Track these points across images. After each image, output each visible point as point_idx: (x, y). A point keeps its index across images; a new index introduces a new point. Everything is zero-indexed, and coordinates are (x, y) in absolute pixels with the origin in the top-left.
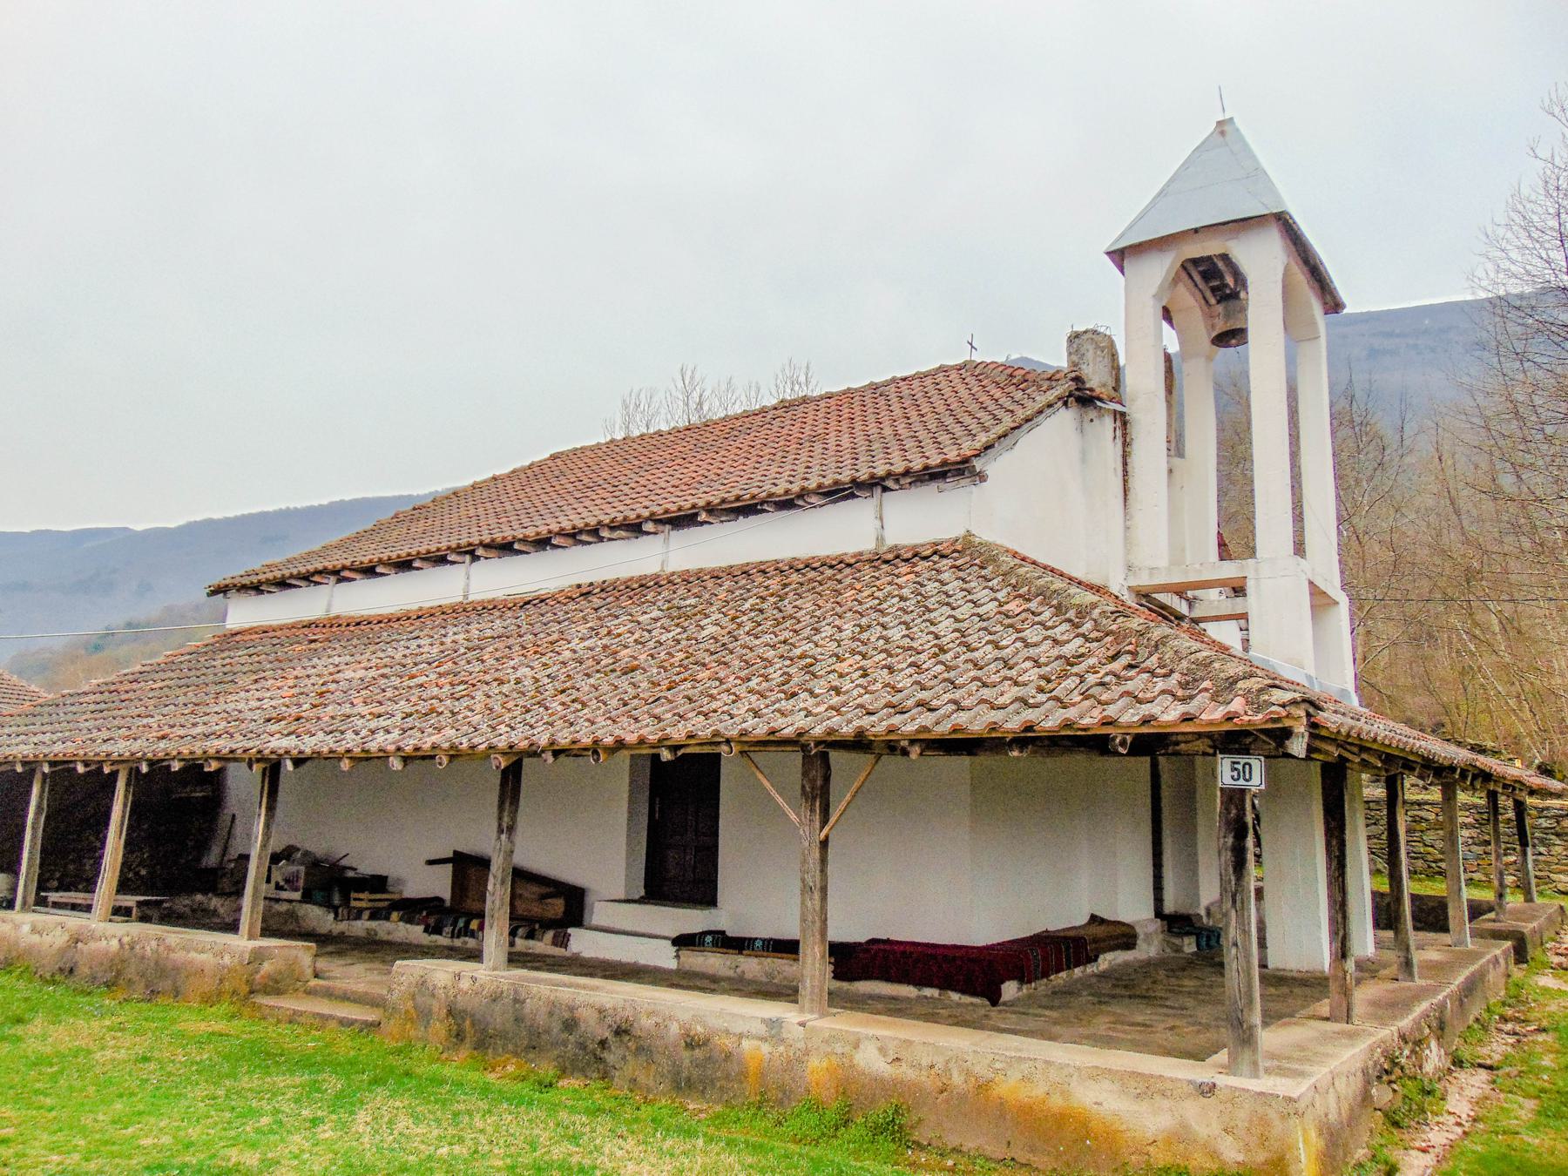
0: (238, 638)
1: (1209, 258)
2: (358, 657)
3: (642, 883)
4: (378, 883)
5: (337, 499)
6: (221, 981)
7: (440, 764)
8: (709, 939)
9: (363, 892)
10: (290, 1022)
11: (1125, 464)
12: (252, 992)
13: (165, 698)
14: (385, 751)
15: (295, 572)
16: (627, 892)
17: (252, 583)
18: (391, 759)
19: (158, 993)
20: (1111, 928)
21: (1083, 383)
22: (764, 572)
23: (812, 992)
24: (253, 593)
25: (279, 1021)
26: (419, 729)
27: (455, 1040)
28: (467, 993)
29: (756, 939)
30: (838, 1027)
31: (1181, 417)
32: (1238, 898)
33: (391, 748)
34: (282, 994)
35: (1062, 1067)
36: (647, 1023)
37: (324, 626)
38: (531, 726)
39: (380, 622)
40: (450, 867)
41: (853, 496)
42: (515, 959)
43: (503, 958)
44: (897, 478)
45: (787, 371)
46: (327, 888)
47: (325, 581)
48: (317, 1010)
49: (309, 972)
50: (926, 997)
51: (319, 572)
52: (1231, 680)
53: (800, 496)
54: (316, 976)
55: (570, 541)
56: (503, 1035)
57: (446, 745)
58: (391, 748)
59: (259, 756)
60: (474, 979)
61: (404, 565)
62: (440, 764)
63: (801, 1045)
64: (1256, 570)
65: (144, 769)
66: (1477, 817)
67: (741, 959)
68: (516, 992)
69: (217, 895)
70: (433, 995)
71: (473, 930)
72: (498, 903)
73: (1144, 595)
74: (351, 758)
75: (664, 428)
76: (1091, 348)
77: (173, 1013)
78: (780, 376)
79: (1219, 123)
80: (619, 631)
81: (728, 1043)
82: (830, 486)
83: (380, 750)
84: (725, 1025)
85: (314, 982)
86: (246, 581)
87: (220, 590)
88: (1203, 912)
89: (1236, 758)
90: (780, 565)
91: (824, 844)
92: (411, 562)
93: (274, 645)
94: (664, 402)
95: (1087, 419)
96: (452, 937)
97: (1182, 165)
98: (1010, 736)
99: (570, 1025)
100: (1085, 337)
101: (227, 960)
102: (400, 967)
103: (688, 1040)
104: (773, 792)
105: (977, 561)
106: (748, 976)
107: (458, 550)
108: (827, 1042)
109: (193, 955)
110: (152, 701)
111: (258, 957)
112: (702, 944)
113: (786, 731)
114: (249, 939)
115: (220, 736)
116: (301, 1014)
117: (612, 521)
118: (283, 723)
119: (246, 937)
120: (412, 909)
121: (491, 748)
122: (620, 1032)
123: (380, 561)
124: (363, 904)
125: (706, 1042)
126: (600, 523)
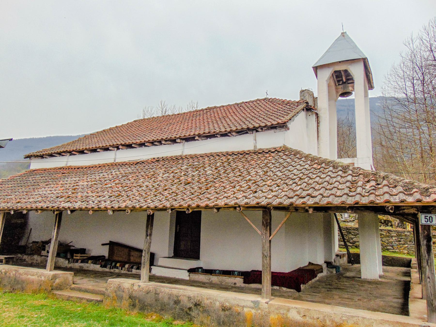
0: (36, 172)
1: (340, 71)
2: (81, 178)
3: (173, 252)
4: (83, 251)
5: (49, 136)
6: (40, 285)
7: (127, 213)
8: (200, 270)
9: (78, 254)
10: (68, 300)
11: (318, 129)
12: (52, 289)
13: (14, 190)
14: (107, 208)
15: (56, 152)
16: (169, 254)
17: (40, 155)
18: (108, 211)
19: (15, 289)
20: (316, 267)
21: (308, 104)
22: (218, 155)
23: (267, 292)
24: (40, 158)
25: (63, 300)
26: (117, 201)
27: (132, 307)
28: (136, 291)
29: (216, 270)
30: (281, 304)
32: (429, 261)
33: (109, 207)
34: (62, 290)
35: (369, 319)
36: (207, 302)
37: (66, 169)
38: (160, 201)
39: (86, 168)
40: (108, 246)
41: (247, 133)
42: (57, 268)
43: (147, 278)
45: (191, 104)
46: (65, 252)
47: (66, 155)
48: (78, 296)
49: (71, 282)
50: (275, 289)
51: (64, 152)
52: (426, 189)
53: (230, 132)
54: (74, 284)
55: (151, 144)
56: (151, 305)
57: (130, 206)
58: (109, 207)
59: (57, 209)
60: (139, 286)
61: (94, 150)
62: (127, 213)
63: (267, 310)
64: (357, 161)
65: (12, 213)
66: (397, 234)
67: (211, 277)
68: (156, 290)
69: (26, 254)
70: (123, 291)
71: (118, 267)
72: (146, 260)
74: (92, 210)
75: (170, 114)
76: (308, 95)
77: (24, 297)
78: (189, 105)
79: (342, 33)
80: (176, 171)
81: (239, 309)
82: (240, 129)
83: (226, 205)
84: (237, 303)
85: (73, 286)
86: (39, 154)
87: (29, 157)
88: (333, 261)
89: (427, 215)
90: (224, 153)
91: (270, 241)
92: (96, 149)
93: (50, 174)
94: (155, 110)
95: (308, 115)
96: (110, 268)
97: (333, 44)
98: (348, 206)
99: (177, 302)
100: (306, 91)
101: (43, 278)
102: (110, 281)
103: (223, 308)
104: (251, 224)
105: (293, 153)
106: (213, 282)
107: (113, 146)
108: (277, 309)
109: (29, 276)
110: (10, 191)
111: (55, 277)
112: (198, 271)
113: (144, 207)
114: (50, 271)
115: (41, 202)
116: (72, 297)
117: (166, 138)
118: (63, 198)
119: (49, 270)
120: (96, 259)
121: (148, 207)
122: (197, 305)
123: (86, 149)
124: (78, 258)
125: (230, 309)
126: (162, 139)
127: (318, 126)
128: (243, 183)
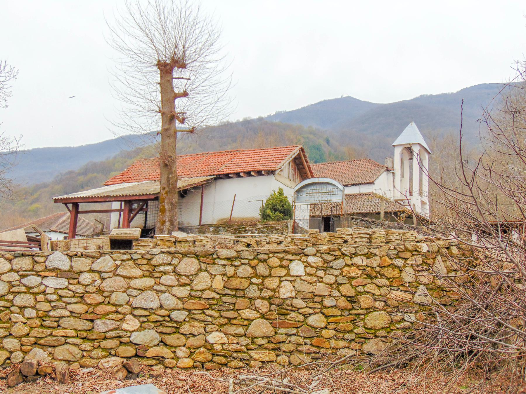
31: (403, 169)
44: (363, 183)
73: (396, 201)
127: (394, 179)
128: (355, 207)
